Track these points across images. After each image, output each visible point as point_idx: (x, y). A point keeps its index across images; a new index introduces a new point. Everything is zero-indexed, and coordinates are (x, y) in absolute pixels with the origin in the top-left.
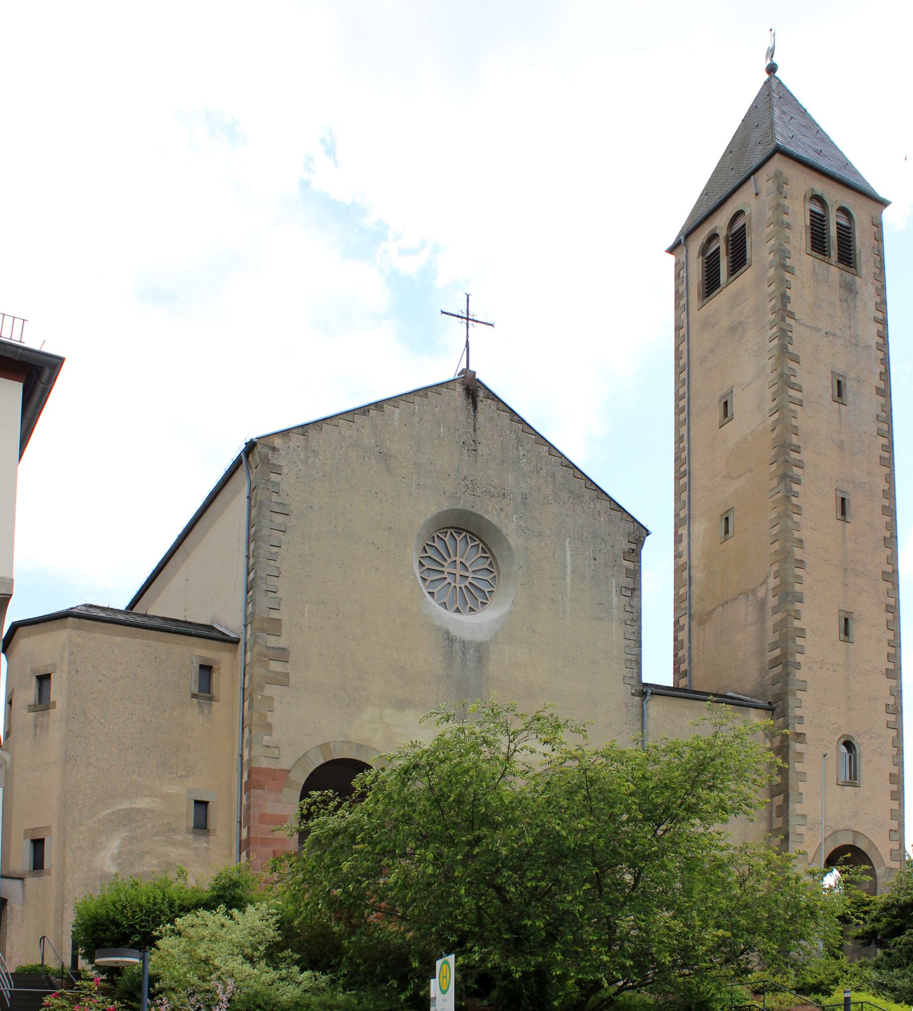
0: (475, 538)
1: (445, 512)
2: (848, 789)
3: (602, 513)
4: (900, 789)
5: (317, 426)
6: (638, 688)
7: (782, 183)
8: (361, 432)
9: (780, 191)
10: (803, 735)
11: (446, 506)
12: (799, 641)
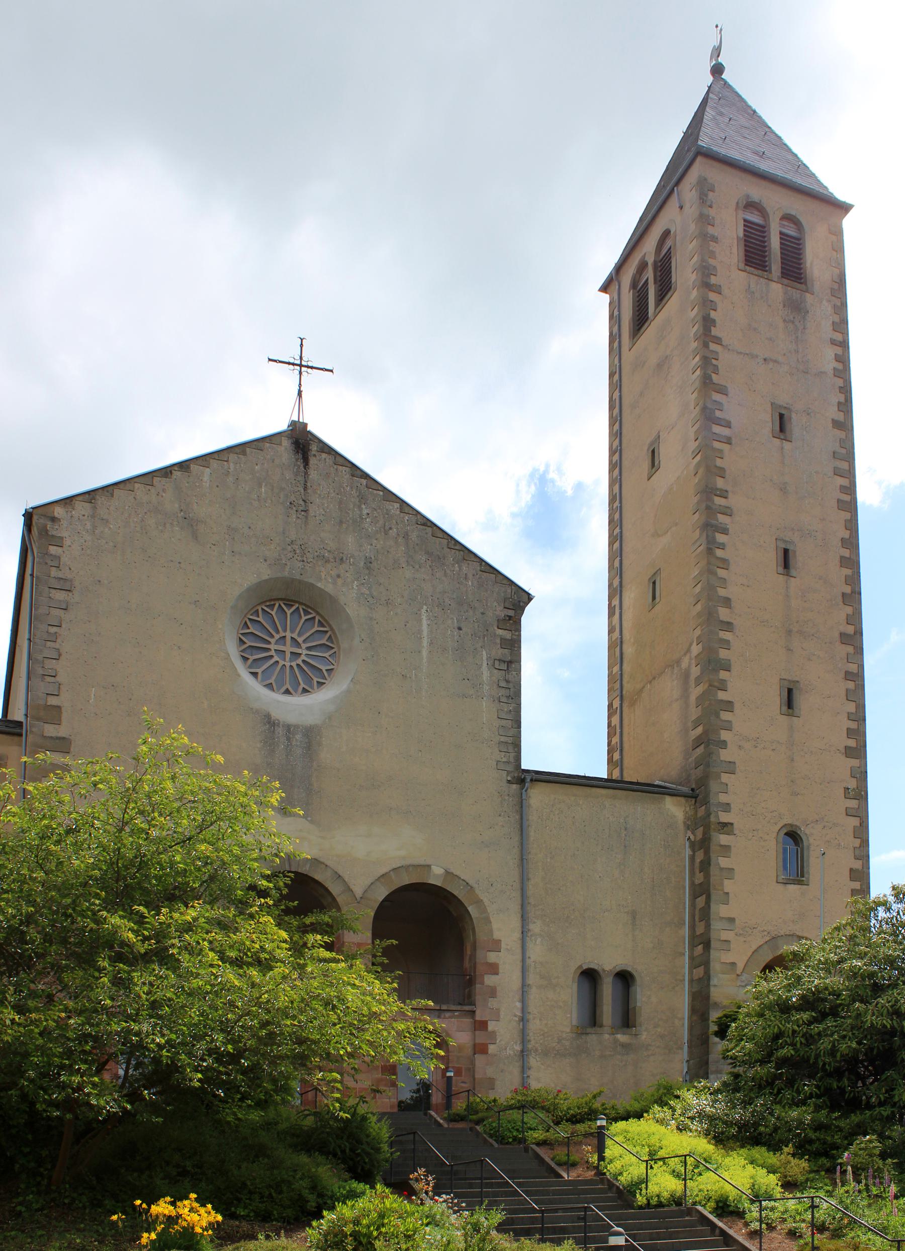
0: (310, 610)
1: (266, 581)
2: (792, 887)
3: (470, 576)
4: (864, 887)
5: (108, 492)
6: (516, 775)
7: (706, 190)
8: (162, 496)
9: (703, 199)
10: (729, 826)
11: (266, 573)
12: (725, 716)
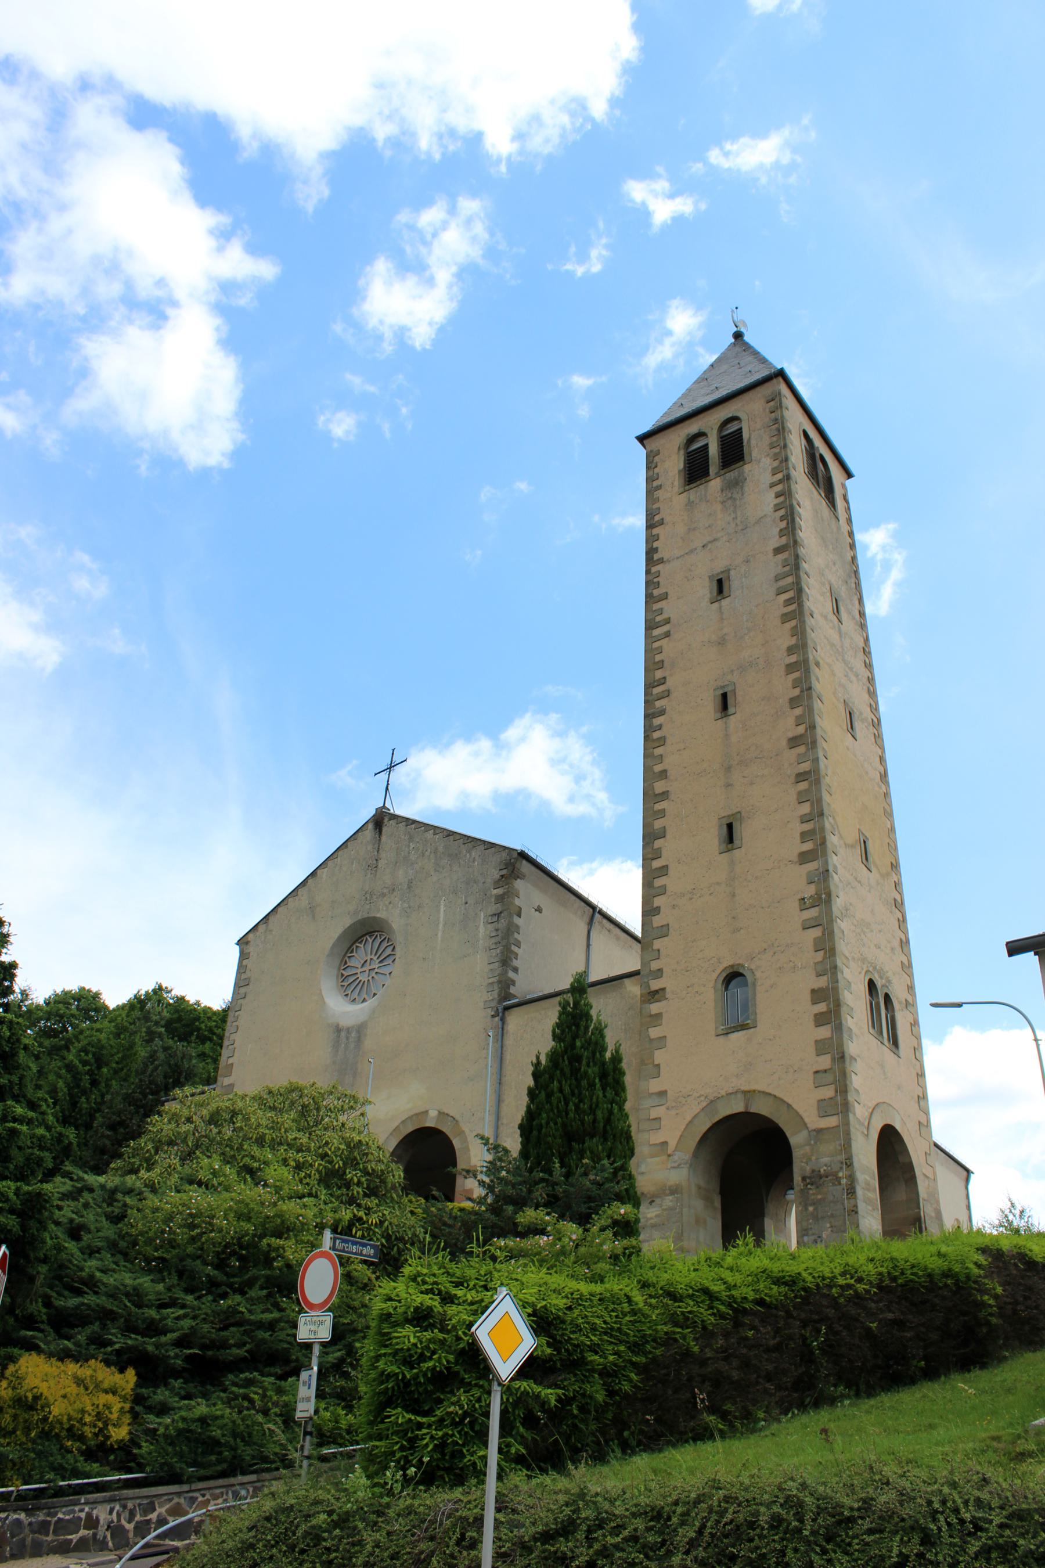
11: (347, 922)
